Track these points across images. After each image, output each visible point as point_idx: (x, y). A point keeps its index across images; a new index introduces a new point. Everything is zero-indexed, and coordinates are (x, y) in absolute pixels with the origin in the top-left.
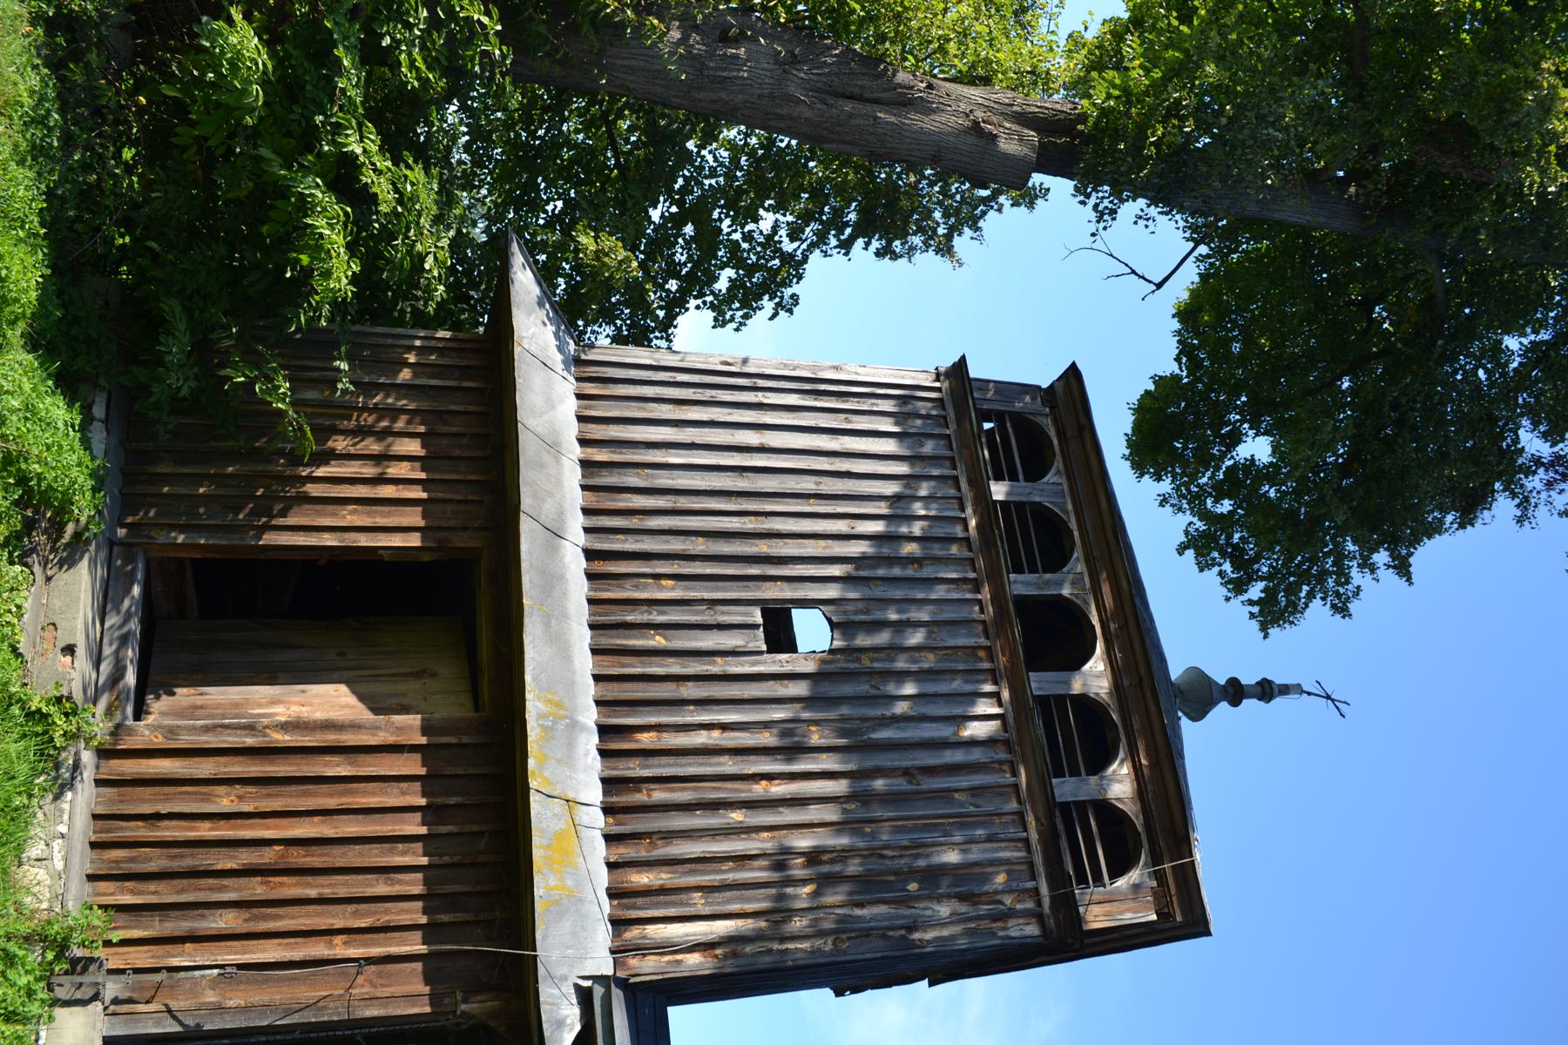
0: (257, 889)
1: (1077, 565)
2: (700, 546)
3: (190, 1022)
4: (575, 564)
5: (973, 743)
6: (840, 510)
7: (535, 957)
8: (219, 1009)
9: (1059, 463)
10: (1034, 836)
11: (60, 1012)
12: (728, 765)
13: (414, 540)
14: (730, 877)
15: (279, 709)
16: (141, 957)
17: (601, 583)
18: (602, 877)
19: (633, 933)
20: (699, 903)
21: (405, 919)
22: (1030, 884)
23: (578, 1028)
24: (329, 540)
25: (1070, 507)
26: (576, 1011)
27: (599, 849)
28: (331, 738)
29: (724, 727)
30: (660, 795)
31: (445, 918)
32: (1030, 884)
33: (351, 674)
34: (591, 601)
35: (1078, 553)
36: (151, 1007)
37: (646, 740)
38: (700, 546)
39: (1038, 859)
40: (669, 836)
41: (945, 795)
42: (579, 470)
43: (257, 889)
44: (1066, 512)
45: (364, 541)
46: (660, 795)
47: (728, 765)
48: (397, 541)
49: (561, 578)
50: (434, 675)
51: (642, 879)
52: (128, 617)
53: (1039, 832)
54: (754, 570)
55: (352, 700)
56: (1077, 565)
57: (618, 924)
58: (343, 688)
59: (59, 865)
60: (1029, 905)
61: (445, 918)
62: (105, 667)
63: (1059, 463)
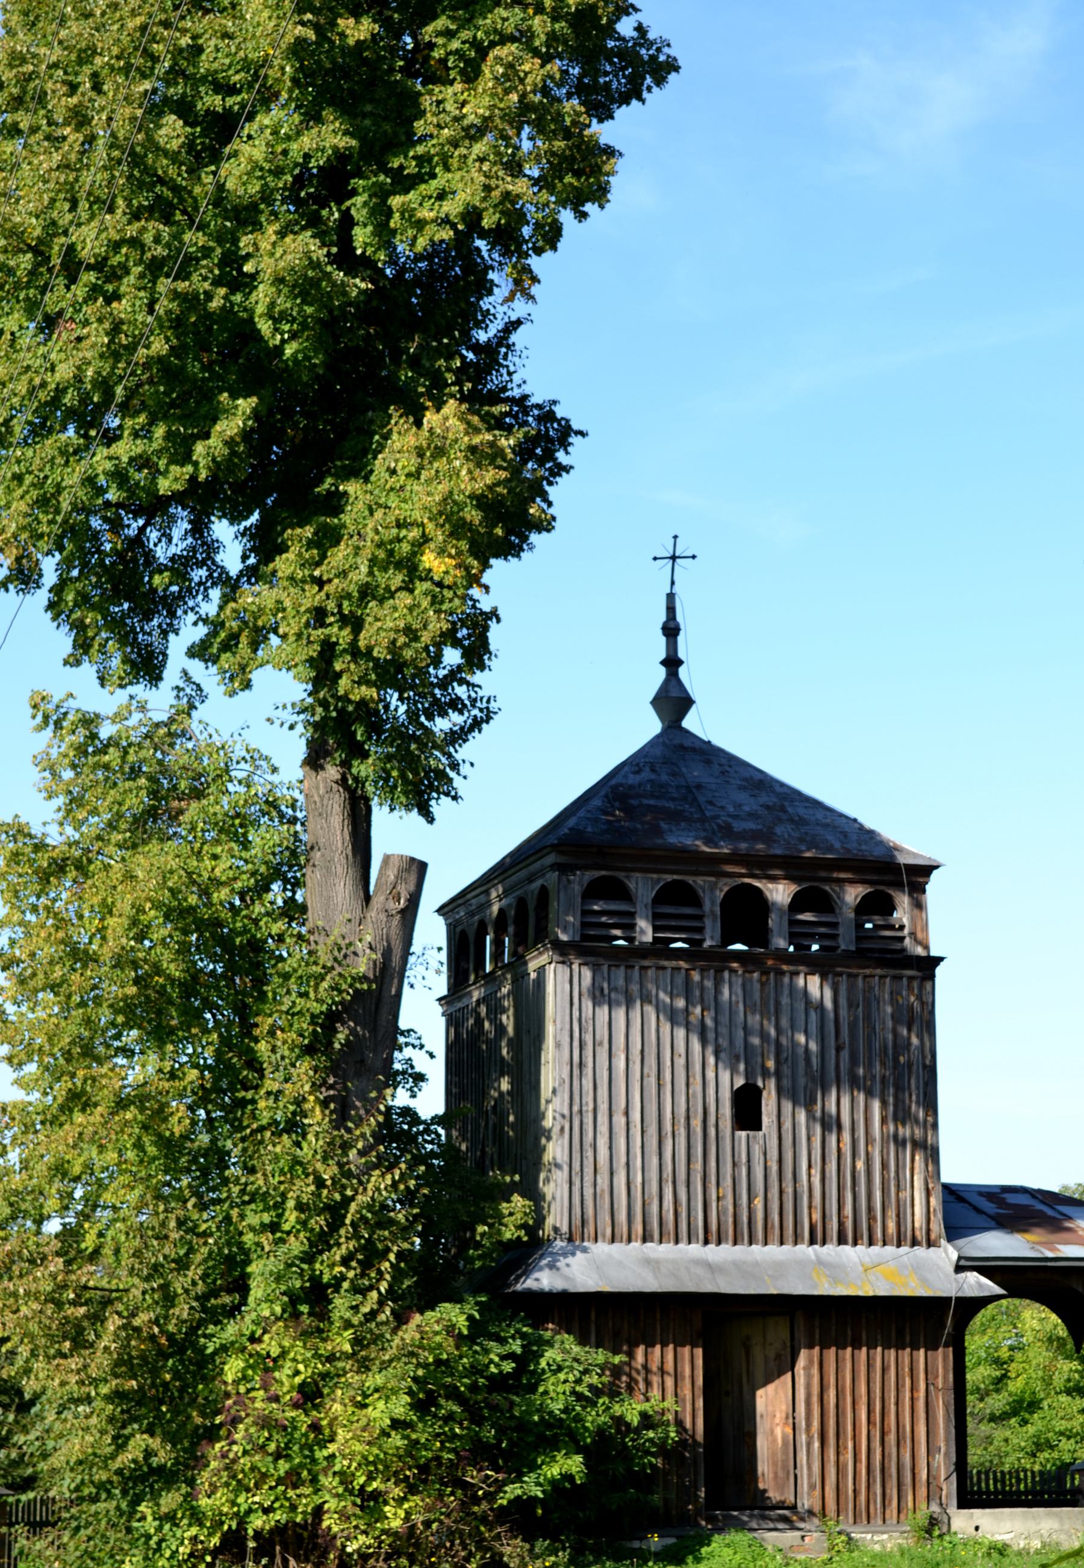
0: (892, 1438)
1: (699, 882)
2: (698, 1166)
3: (953, 1468)
4: (714, 1253)
5: (835, 1001)
6: (669, 1063)
7: (957, 1299)
8: (946, 1454)
9: (621, 875)
10: (879, 971)
11: (953, 1529)
12: (832, 1167)
13: (699, 1352)
14: (892, 1174)
15: (778, 1432)
16: (922, 1492)
17: (723, 1236)
18: (890, 1249)
19: (920, 1235)
20: (905, 1195)
21: (907, 1361)
22: (905, 980)
23: (975, 1274)
24: (700, 1403)
25: (655, 876)
26: (969, 1274)
27: (876, 1249)
28: (815, 1399)
29: (810, 1167)
30: (848, 1210)
31: (908, 1339)
32: (905, 980)
33: (745, 1388)
34: (735, 1243)
35: (690, 880)
36: (944, 1487)
37: (817, 1216)
38: (698, 1166)
39: (892, 972)
40: (870, 1209)
41: (853, 1026)
42: (649, 1244)
43: (892, 1438)
44: (658, 880)
45: (700, 1381)
46: (848, 1210)
47: (832, 1167)
48: (699, 1362)
49: (735, 1263)
50: (748, 1338)
51: (892, 1226)
52: (751, 1516)
53: (876, 968)
54: (712, 1132)
55: (771, 1388)
56: (699, 882)
57: (914, 1243)
58: (760, 1393)
59: (885, 1536)
60: (915, 984)
61: (908, 1339)
62: (780, 1526)
63: (621, 875)
